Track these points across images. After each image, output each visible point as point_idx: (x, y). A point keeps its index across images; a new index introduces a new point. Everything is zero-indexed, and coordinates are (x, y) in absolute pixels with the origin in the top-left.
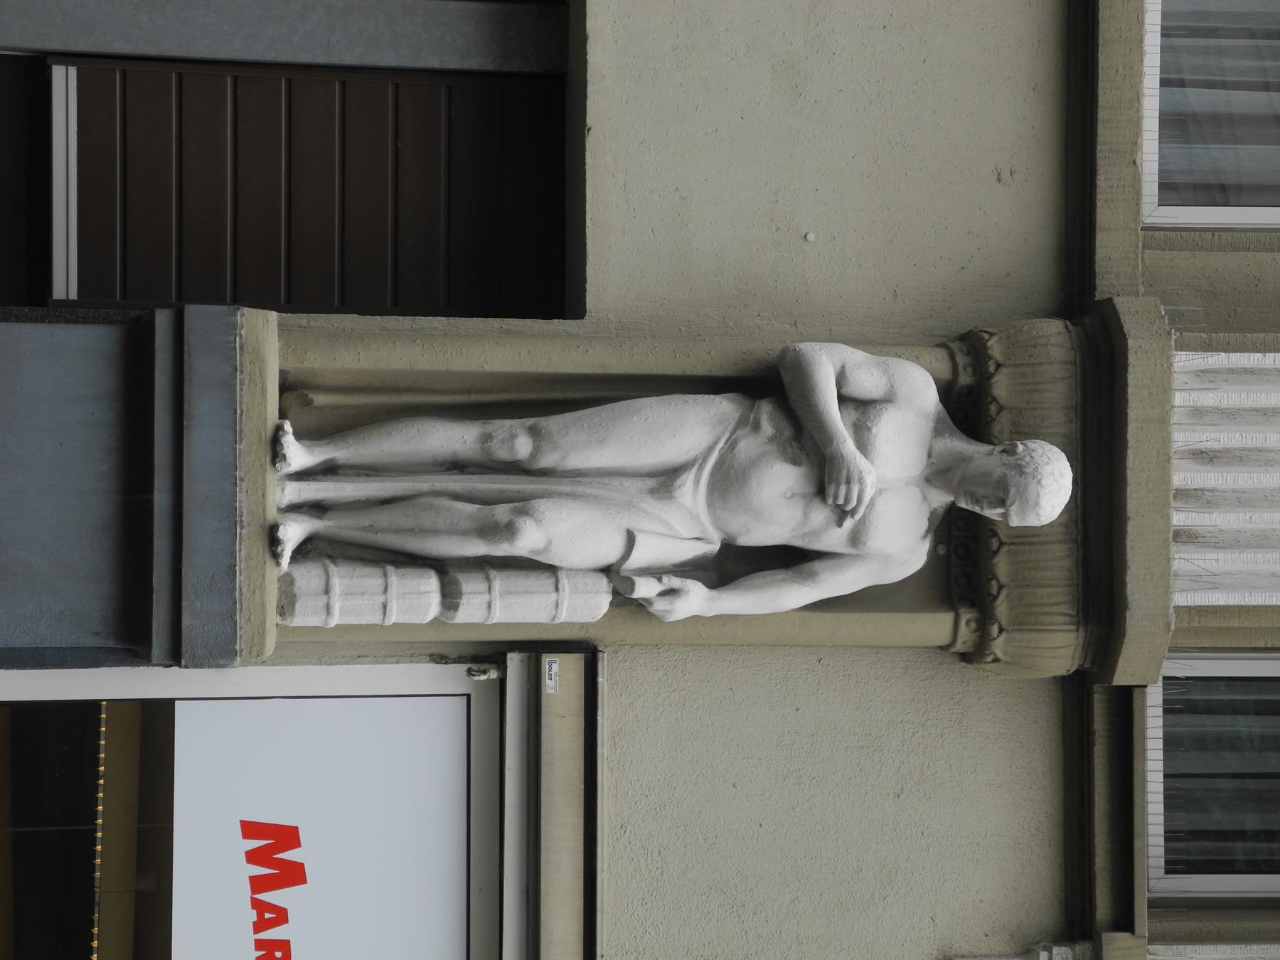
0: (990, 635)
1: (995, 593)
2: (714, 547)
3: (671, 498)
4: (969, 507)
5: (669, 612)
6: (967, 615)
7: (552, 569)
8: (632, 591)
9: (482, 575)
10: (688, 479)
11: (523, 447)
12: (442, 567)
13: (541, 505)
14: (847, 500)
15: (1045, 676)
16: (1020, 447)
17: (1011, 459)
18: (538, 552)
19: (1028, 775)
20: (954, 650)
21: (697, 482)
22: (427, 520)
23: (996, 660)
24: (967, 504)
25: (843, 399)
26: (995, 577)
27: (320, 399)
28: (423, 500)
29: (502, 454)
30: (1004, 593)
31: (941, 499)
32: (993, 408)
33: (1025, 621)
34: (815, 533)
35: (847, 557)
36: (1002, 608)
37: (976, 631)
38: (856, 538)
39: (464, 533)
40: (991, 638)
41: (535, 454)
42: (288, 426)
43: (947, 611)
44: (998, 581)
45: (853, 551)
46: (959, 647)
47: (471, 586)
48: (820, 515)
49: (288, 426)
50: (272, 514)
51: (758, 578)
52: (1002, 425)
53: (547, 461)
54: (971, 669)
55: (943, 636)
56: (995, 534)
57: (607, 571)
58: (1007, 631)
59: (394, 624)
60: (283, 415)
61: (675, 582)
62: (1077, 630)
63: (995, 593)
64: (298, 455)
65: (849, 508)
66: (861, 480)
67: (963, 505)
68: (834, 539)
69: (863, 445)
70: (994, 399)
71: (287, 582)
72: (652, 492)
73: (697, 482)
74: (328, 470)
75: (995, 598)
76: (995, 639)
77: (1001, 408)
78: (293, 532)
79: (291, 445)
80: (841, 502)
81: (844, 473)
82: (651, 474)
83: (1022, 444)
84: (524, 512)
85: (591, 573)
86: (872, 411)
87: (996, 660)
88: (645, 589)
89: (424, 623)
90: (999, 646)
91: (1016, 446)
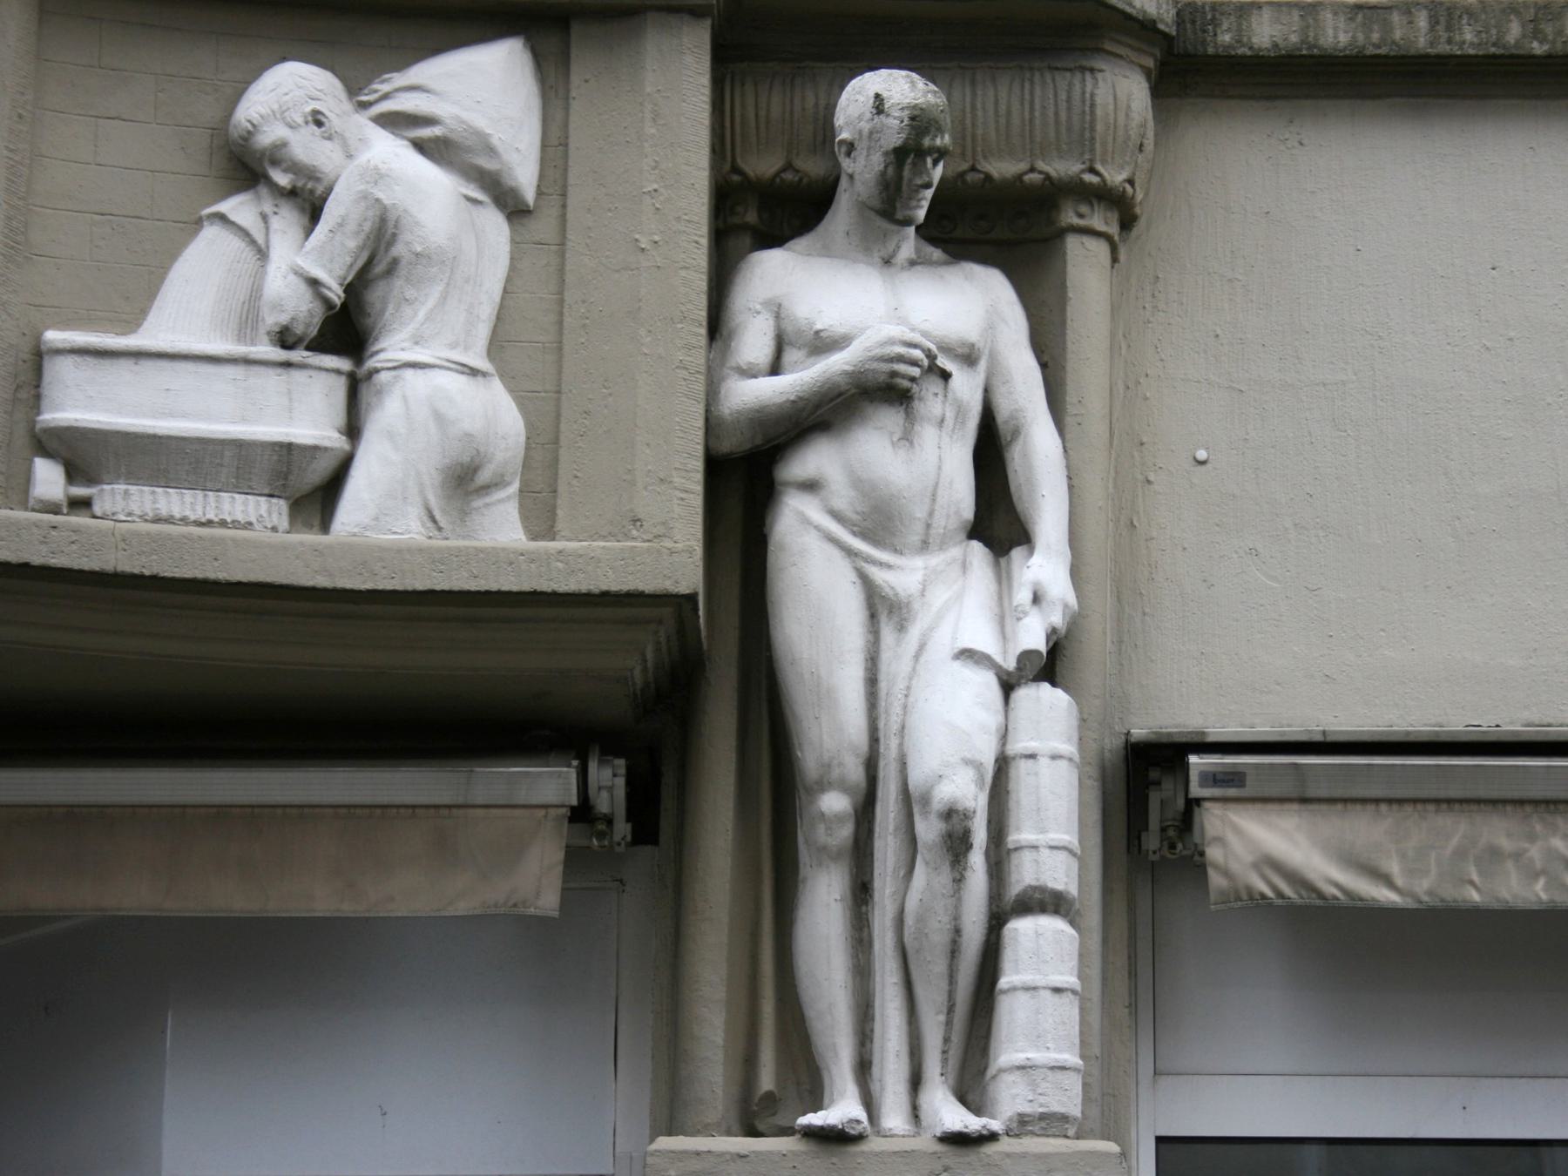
0: (1099, 185)
1: (1042, 176)
2: (976, 546)
3: (908, 604)
4: (926, 204)
5: (1066, 606)
6: (1069, 217)
7: (1003, 764)
8: (1036, 652)
9: (1015, 858)
10: (879, 575)
11: (835, 803)
12: (996, 922)
13: (916, 777)
14: (914, 363)
15: (1153, 125)
16: (844, 135)
17: (861, 147)
18: (981, 778)
19: (1155, 443)
20: (1116, 238)
21: (881, 564)
22: (939, 936)
23: (1131, 182)
24: (922, 207)
25: (775, 369)
26: (1019, 177)
27: (767, 1081)
28: (907, 939)
29: (846, 832)
30: (1041, 165)
31: (909, 243)
32: (789, 176)
33: (1083, 137)
34: (960, 412)
35: (374, 296)
36: (1063, 167)
37: (1092, 205)
38: (969, 358)
39: (959, 880)
40: (1102, 184)
41: (844, 787)
42: (805, 1120)
43: (1063, 242)
44: (1026, 173)
45: (982, 365)
46: (1113, 230)
47: (1027, 873)
48: (931, 402)
49: (805, 1120)
50: (925, 1143)
51: (1019, 508)
52: (813, 167)
53: (854, 771)
54: (1141, 224)
55: (1100, 249)
56: (962, 175)
57: (1008, 686)
58: (1091, 161)
59: (1080, 977)
60: (787, 1131)
61: (1023, 596)
62: (1092, 70)
63: (1042, 176)
64: (842, 1109)
65: (926, 362)
66: (891, 342)
67: (921, 214)
68: (966, 386)
69: (822, 344)
70: (777, 174)
71: (1023, 1125)
72: (901, 628)
73: (881, 564)
74: (864, 1068)
75: (1048, 177)
76: (1104, 181)
77: (788, 166)
78: (953, 1117)
79: (842, 1109)
80: (916, 372)
81: (875, 365)
82: (873, 616)
83: (840, 134)
84: (926, 800)
85: (1012, 705)
86: (789, 328)
87: (1131, 182)
88: (1033, 636)
89: (1076, 935)
90: (1115, 177)
91: (842, 142)
